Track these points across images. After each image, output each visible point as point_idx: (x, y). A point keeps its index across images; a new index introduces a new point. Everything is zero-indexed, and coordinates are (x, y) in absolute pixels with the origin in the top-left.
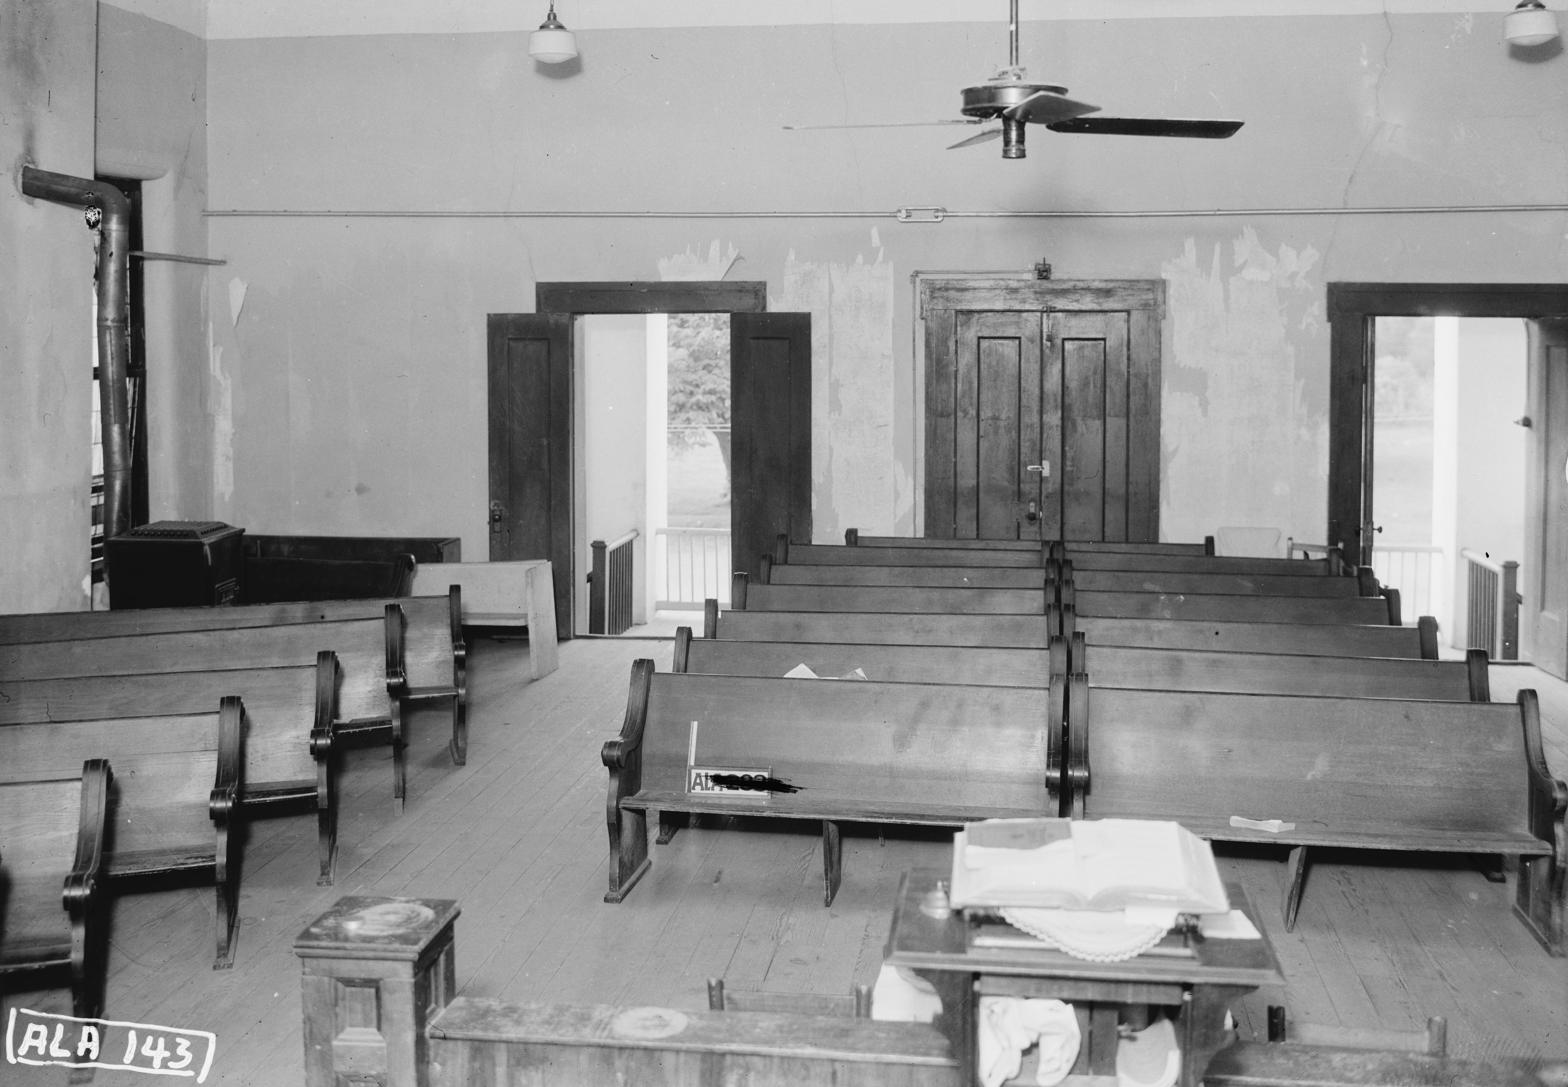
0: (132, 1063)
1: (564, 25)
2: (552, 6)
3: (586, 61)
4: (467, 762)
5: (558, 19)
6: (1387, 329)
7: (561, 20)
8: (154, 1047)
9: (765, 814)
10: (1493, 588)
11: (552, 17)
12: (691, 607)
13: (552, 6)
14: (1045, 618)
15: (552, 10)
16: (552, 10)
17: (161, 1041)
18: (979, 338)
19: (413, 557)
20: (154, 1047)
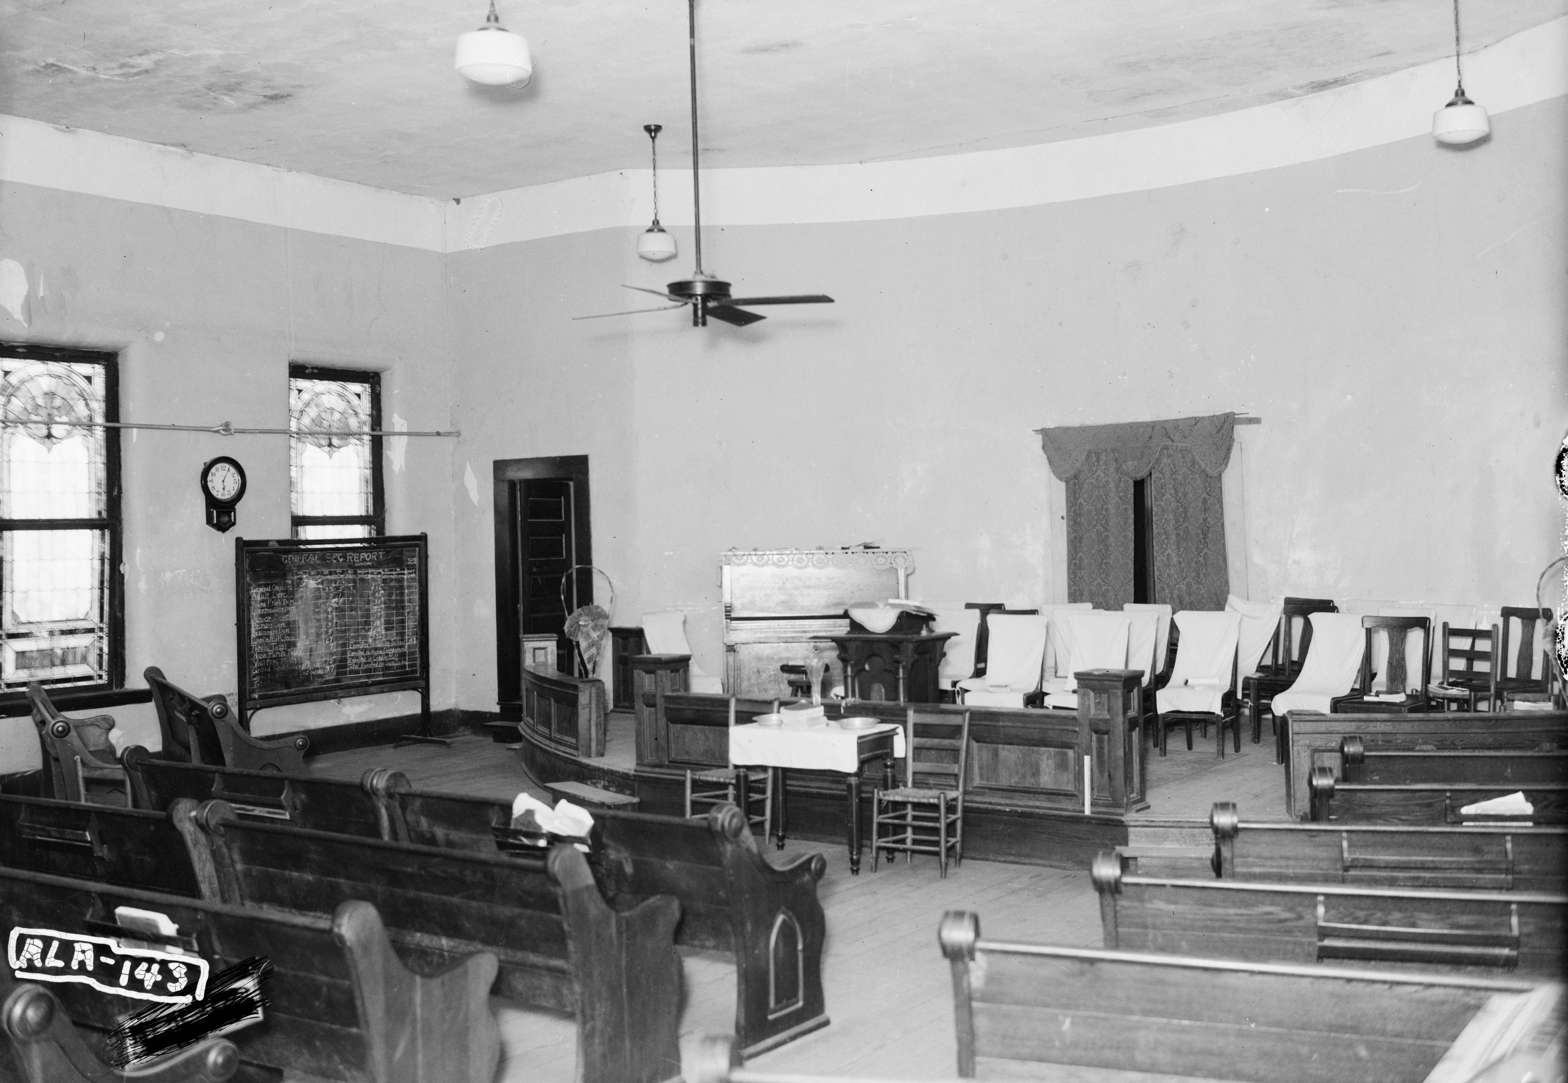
0: (127, 987)
1: (1473, 100)
2: (1460, 82)
3: (1496, 136)
4: (606, 753)
5: (1466, 94)
6: (98, 371)
7: (1469, 95)
8: (148, 970)
9: (106, 649)
10: (1310, 715)
11: (1459, 93)
12: (9, 486)
13: (1460, 82)
14: (1044, 690)
15: (1460, 86)
16: (1460, 86)
17: (155, 967)
18: (109, 360)
19: (666, 553)
20: (148, 970)
